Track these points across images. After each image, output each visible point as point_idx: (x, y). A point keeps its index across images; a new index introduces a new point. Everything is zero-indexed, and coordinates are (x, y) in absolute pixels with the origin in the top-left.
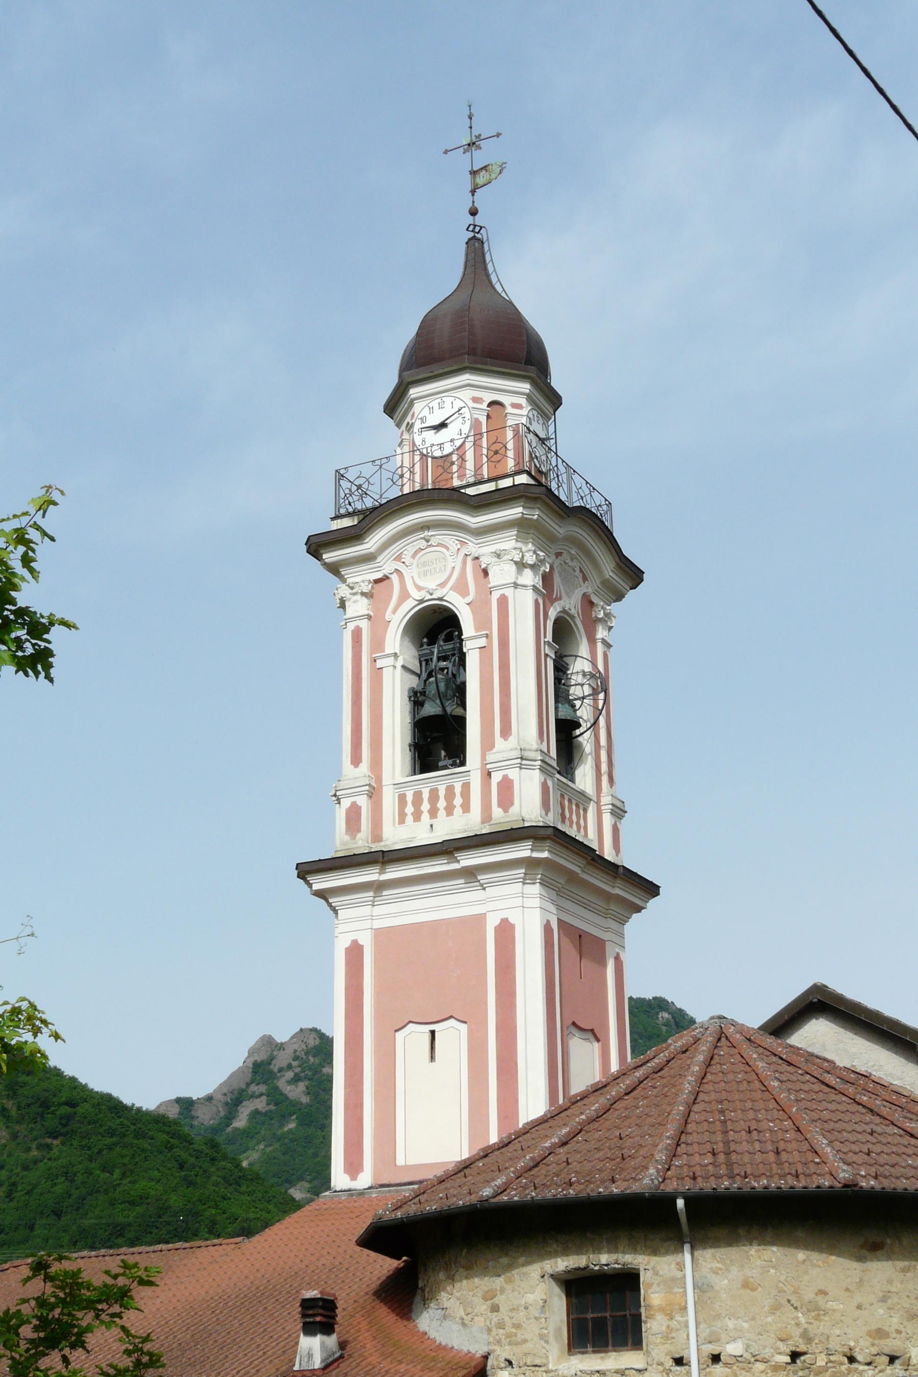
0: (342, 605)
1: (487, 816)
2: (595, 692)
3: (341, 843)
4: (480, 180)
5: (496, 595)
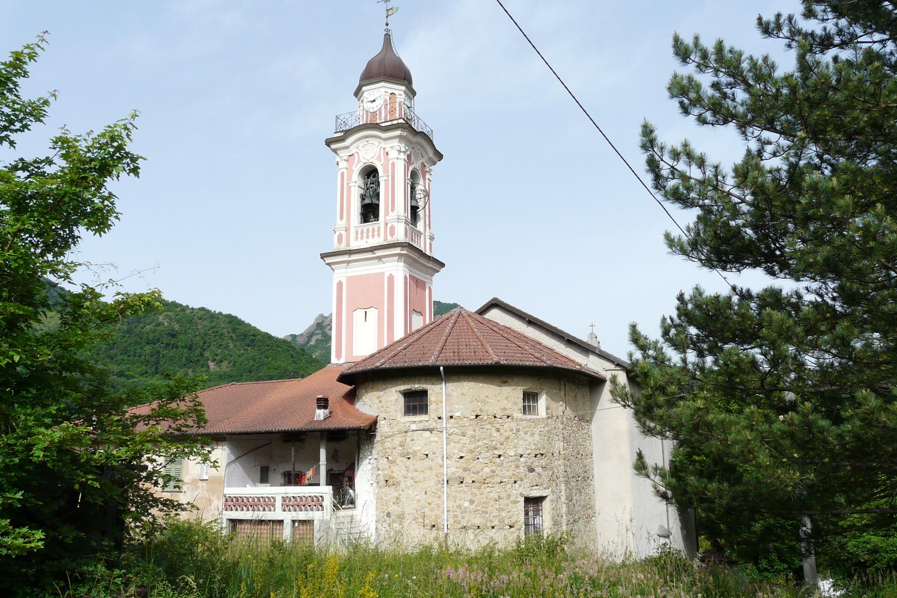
0: (338, 164)
1: (386, 239)
2: (425, 197)
3: (336, 247)
4: (390, 13)
5: (391, 162)
